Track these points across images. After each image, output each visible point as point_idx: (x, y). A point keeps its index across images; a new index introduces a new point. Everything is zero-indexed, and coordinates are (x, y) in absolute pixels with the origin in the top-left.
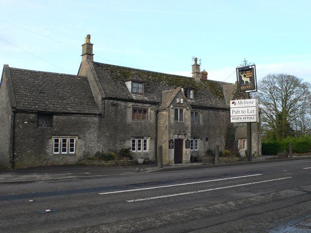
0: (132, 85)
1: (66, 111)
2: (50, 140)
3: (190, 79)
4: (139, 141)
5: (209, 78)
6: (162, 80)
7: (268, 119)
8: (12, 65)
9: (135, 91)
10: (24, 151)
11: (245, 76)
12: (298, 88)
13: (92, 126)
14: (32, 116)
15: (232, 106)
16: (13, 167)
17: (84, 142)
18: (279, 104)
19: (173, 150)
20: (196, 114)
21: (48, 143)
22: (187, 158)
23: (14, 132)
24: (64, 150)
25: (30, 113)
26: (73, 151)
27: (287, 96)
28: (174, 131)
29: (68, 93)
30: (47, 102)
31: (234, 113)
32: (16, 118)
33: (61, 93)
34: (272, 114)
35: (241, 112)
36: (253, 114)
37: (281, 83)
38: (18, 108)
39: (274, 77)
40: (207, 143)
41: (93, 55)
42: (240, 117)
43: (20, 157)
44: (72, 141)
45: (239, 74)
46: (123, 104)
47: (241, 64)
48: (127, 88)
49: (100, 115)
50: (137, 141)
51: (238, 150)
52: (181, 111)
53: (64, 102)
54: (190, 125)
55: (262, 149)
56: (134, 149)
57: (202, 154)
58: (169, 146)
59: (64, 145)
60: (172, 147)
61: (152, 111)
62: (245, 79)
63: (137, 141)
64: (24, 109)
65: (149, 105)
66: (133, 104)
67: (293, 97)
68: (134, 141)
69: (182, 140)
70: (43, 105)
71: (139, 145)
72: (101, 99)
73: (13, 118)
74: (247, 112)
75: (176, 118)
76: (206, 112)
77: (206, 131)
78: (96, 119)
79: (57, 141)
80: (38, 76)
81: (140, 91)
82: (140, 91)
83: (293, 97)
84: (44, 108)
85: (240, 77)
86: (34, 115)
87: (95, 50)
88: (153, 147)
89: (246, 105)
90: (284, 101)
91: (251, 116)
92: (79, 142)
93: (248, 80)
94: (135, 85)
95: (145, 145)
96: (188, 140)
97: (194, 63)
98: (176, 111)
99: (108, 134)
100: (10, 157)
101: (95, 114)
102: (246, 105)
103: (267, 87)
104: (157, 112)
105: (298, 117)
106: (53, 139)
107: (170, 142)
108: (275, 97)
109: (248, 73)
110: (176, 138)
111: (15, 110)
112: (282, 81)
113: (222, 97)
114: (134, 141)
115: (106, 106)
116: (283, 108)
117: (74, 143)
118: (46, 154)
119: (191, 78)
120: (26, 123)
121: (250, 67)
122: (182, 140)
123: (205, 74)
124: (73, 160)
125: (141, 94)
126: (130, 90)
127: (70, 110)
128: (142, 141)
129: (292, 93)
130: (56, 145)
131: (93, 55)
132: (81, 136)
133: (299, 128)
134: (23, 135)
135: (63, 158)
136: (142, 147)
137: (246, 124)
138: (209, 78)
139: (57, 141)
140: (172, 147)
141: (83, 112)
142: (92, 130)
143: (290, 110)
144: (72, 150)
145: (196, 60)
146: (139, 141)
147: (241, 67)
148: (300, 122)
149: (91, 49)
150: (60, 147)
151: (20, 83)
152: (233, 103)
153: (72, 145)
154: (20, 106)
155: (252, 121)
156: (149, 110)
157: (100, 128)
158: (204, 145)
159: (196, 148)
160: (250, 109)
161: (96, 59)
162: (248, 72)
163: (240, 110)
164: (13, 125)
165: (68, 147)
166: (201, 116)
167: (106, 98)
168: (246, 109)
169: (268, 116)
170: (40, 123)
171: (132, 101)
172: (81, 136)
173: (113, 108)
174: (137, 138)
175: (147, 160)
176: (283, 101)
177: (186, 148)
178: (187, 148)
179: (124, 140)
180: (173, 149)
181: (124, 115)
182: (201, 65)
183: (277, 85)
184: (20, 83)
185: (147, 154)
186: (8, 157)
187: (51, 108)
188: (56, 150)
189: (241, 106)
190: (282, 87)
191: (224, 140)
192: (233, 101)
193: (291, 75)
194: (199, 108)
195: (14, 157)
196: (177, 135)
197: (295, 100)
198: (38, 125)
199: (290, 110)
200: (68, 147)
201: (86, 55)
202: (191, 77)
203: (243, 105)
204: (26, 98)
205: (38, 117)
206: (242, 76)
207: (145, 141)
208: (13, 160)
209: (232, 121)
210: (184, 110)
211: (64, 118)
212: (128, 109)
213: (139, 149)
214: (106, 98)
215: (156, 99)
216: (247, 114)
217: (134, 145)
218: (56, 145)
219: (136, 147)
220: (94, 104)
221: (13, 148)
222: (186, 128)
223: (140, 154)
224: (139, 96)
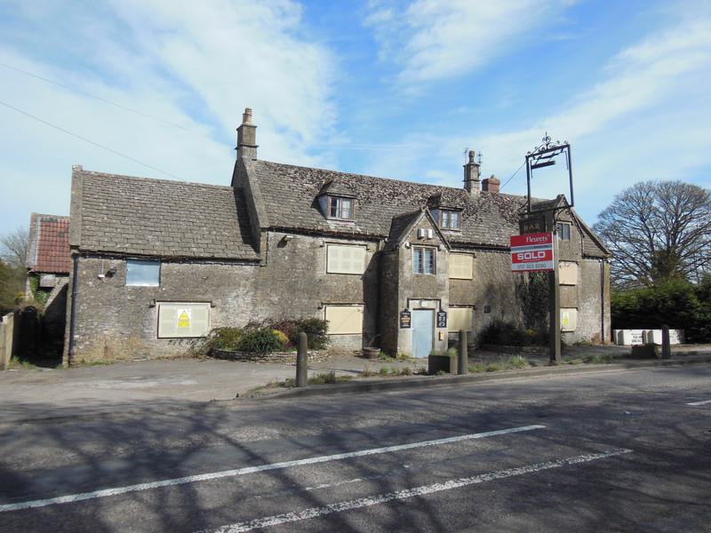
7: (638, 269)
12: (702, 208)
13: (242, 282)
18: (661, 240)
27: (677, 228)
29: (199, 219)
34: (645, 260)
37: (666, 200)
39: (651, 189)
43: (87, 343)
46: (309, 239)
55: (440, 438)
67: (691, 226)
78: (249, 269)
83: (691, 226)
87: (260, 138)
90: (673, 233)
103: (635, 210)
105: (702, 264)
108: (650, 227)
127: (196, 251)
129: (688, 219)
141: (225, 256)
142: (241, 291)
145: (471, 155)
169: (635, 263)
172: (217, 302)
176: (668, 233)
183: (656, 204)
193: (688, 182)
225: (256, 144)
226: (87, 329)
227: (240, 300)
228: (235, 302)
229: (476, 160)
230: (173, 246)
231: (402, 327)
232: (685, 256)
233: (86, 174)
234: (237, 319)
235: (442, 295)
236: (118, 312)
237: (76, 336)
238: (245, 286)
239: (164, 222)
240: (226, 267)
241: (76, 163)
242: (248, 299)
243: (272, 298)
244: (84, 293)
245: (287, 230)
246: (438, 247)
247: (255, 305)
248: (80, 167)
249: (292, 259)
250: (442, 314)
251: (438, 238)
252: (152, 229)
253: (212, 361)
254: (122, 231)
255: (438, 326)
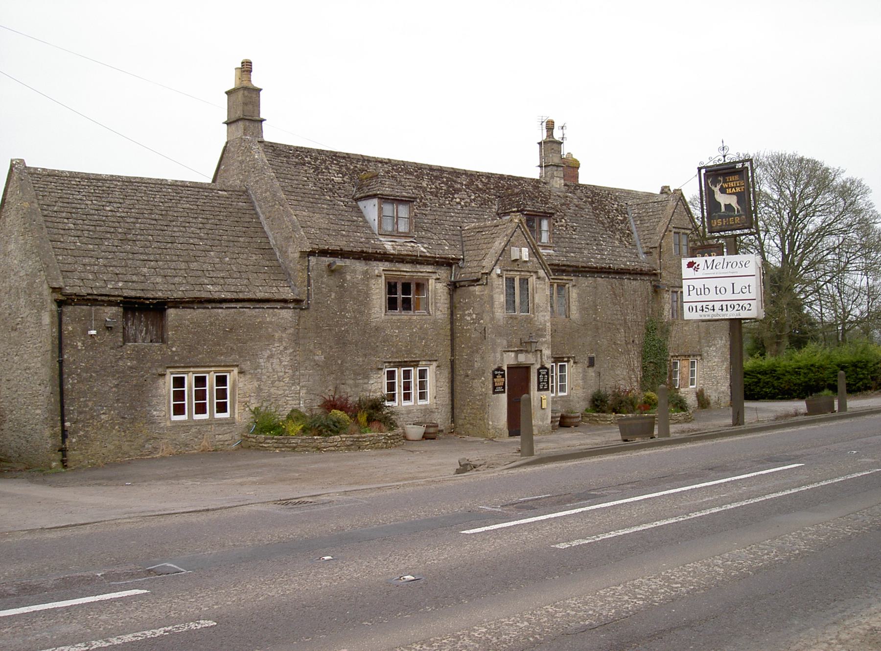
0: (380, 210)
1: (204, 295)
2: (161, 381)
3: (535, 183)
4: (407, 374)
5: (585, 178)
6: (457, 191)
8: (36, 161)
9: (389, 227)
10: (93, 417)
11: (723, 191)
14: (110, 313)
15: (687, 272)
16: (64, 463)
17: (256, 384)
19: (504, 397)
20: (561, 287)
21: (157, 388)
22: (543, 420)
23: (61, 363)
24: (201, 409)
25: (103, 303)
26: (205, 412)
28: (505, 342)
30: (145, 270)
31: (693, 293)
32: (64, 318)
33: (182, 240)
35: (713, 290)
36: (747, 296)
37: (779, 180)
38: (68, 290)
40: (591, 372)
41: (262, 121)
42: (711, 304)
43: (82, 433)
44: (221, 380)
45: (706, 184)
46: (359, 266)
47: (712, 157)
48: (366, 221)
49: (297, 301)
50: (399, 373)
51: (677, 390)
52: (524, 282)
53: (194, 266)
54: (548, 324)
56: (392, 398)
57: (580, 406)
58: (494, 388)
59: (201, 395)
60: (500, 389)
61: (440, 286)
62: (723, 199)
63: (399, 373)
64: (84, 292)
65: (430, 269)
66: (387, 265)
68: (391, 375)
69: (527, 369)
70: (135, 278)
71: (407, 387)
72: (297, 255)
73: (56, 319)
74: (730, 290)
75: (510, 303)
76: (586, 282)
77: (589, 339)
78: (287, 314)
79: (179, 382)
80: (109, 191)
81: (403, 227)
82: (403, 227)
84: (140, 286)
85: (710, 194)
86: (114, 309)
88: (445, 389)
89: (729, 271)
91: (741, 303)
92: (241, 385)
93: (733, 201)
94: (388, 209)
95: (422, 385)
96: (543, 367)
97: (543, 136)
98: (510, 281)
99: (320, 357)
100: (54, 436)
101: (285, 301)
102: (729, 271)
104: (454, 287)
106: (170, 379)
107: (495, 376)
109: (734, 182)
110: (512, 362)
111: (61, 298)
112: (782, 176)
113: (628, 235)
114: (391, 375)
115: (312, 274)
116: (785, 257)
117: (228, 387)
118: (152, 422)
119: (538, 181)
120: (93, 332)
121: (739, 166)
122: (527, 369)
123: (571, 168)
124: (227, 437)
125: (405, 235)
126: (375, 225)
127: (213, 291)
128: (414, 373)
130: (179, 396)
131: (262, 121)
132: (247, 366)
133: (829, 315)
134: (86, 370)
135: (199, 432)
136: (414, 391)
137: (728, 323)
138: (585, 178)
139: (179, 382)
140: (500, 389)
141: (251, 296)
142: (277, 347)
143: (805, 263)
144: (222, 408)
145: (550, 126)
146: (407, 374)
147: (711, 164)
148: (833, 296)
149: (256, 104)
150: (191, 401)
151: (64, 215)
152: (690, 265)
153: (222, 394)
154: (73, 287)
155: (744, 314)
156: (432, 282)
157: (296, 339)
158: (584, 378)
159: (562, 389)
160: (740, 283)
161: (271, 133)
162: (732, 178)
163: (711, 284)
164: (57, 342)
165: (211, 400)
166: (574, 294)
167: (312, 253)
168: (727, 282)
170: (132, 332)
171: (384, 257)
172: (247, 366)
173: (332, 281)
174: (399, 365)
175: (432, 430)
177: (539, 390)
178: (543, 390)
179: (365, 374)
180: (506, 394)
181: (364, 300)
182: (565, 142)
184: (64, 215)
185: (427, 411)
186: (47, 433)
187: (160, 289)
188: (179, 410)
189: (710, 272)
190: (781, 193)
191: (636, 363)
192: (691, 260)
193: (807, 156)
194: (568, 273)
195: (64, 434)
196: (513, 354)
197: (822, 232)
198: (126, 339)
199: (805, 263)
200: (211, 400)
201: (241, 124)
202: (537, 177)
203: (720, 272)
204: (87, 260)
205: (125, 315)
206: (716, 189)
207: (422, 374)
208: (63, 442)
209: (688, 315)
210: (532, 280)
211: (198, 314)
212: (373, 281)
213: (407, 397)
214: (312, 253)
215: (448, 251)
216: (729, 295)
217: (391, 387)
218: (179, 396)
219: (399, 391)
220: (281, 272)
221: (62, 407)
222: (540, 332)
223: (409, 411)
224: (401, 241)
225: (262, 116)
226: (80, 413)
227: (275, 361)
228: (269, 365)
229: (557, 135)
230: (180, 284)
231: (494, 393)
232: (806, 269)
233: (33, 173)
234: (272, 390)
235: (542, 343)
236: (117, 386)
237: (67, 424)
238: (280, 340)
239: (155, 245)
240: (254, 312)
241: (17, 156)
242: (286, 360)
243: (317, 358)
244: (71, 359)
245: (334, 254)
246: (536, 272)
247: (295, 368)
248: (22, 161)
249: (340, 298)
250: (543, 372)
251: (535, 259)
252: (142, 257)
253: (425, 441)
254: (105, 262)
255: (539, 390)
